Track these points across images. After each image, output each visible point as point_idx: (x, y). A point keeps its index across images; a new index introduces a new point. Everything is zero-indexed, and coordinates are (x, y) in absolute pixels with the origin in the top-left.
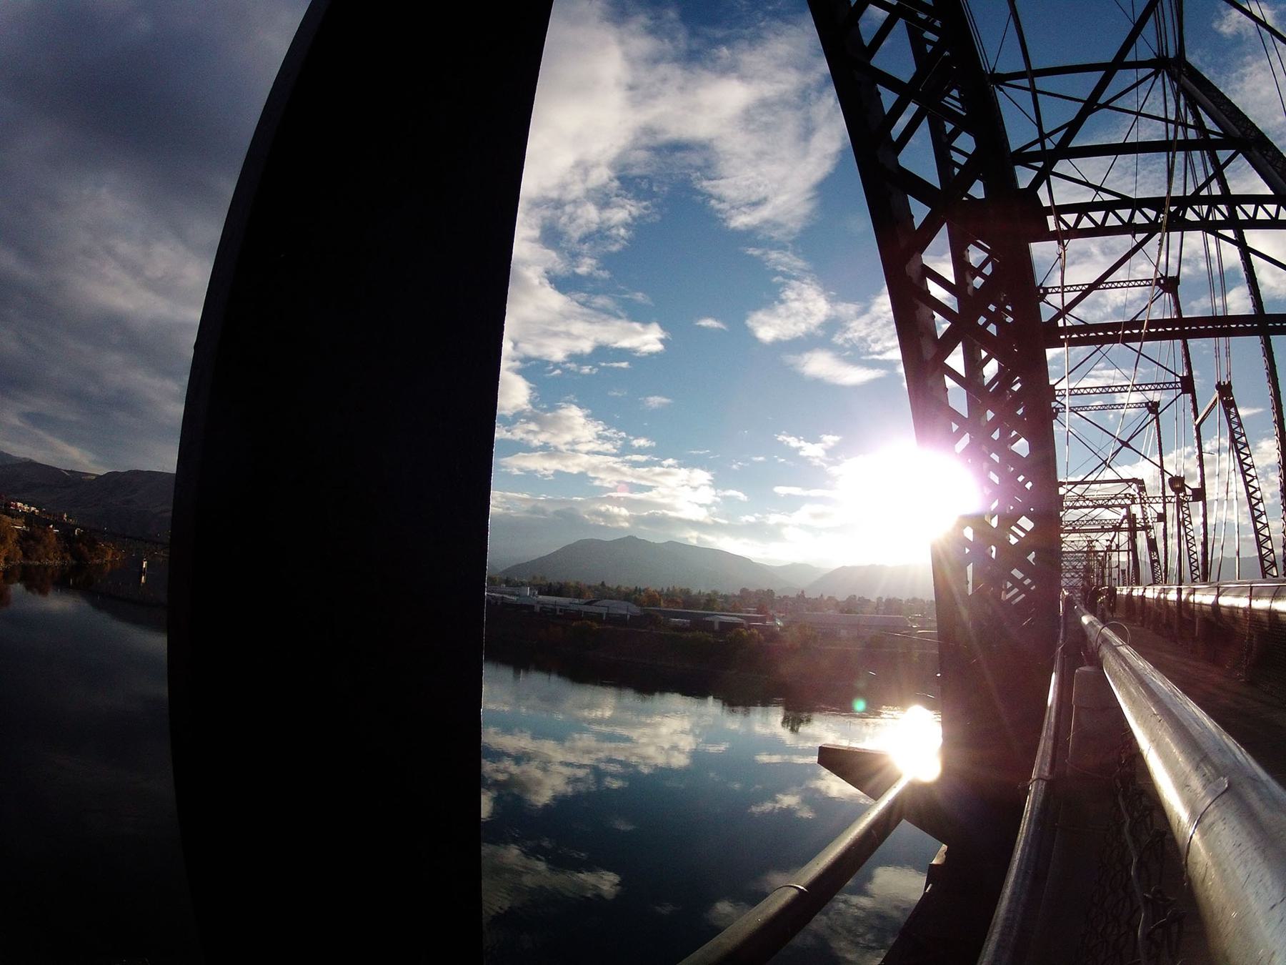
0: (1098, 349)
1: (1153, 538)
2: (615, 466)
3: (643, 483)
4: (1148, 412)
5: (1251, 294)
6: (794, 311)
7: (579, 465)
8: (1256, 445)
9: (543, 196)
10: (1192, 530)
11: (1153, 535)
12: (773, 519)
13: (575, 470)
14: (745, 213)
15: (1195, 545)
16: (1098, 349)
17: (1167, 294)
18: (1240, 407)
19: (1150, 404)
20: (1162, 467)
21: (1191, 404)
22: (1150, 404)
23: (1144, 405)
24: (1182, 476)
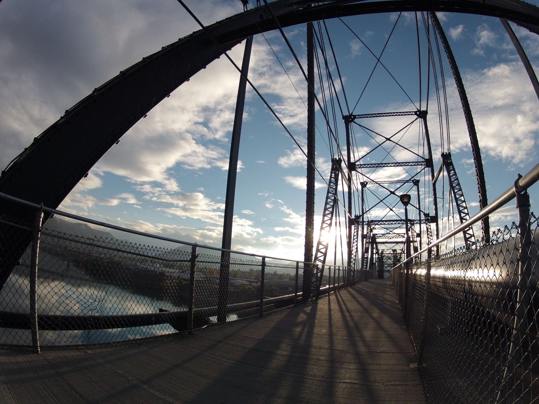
0: (413, 177)
1: (416, 246)
2: (212, 217)
3: (218, 223)
4: (413, 185)
5: (463, 106)
6: (198, 116)
7: (197, 215)
8: (184, 206)
9: (206, 106)
10: (432, 239)
11: (416, 245)
12: (272, 239)
13: (196, 218)
14: (288, 119)
15: (432, 239)
16: (413, 177)
17: (421, 119)
18: (473, 163)
19: (415, 181)
20: (419, 209)
21: (434, 211)
22: (415, 181)
23: (411, 181)
24: (428, 213)
